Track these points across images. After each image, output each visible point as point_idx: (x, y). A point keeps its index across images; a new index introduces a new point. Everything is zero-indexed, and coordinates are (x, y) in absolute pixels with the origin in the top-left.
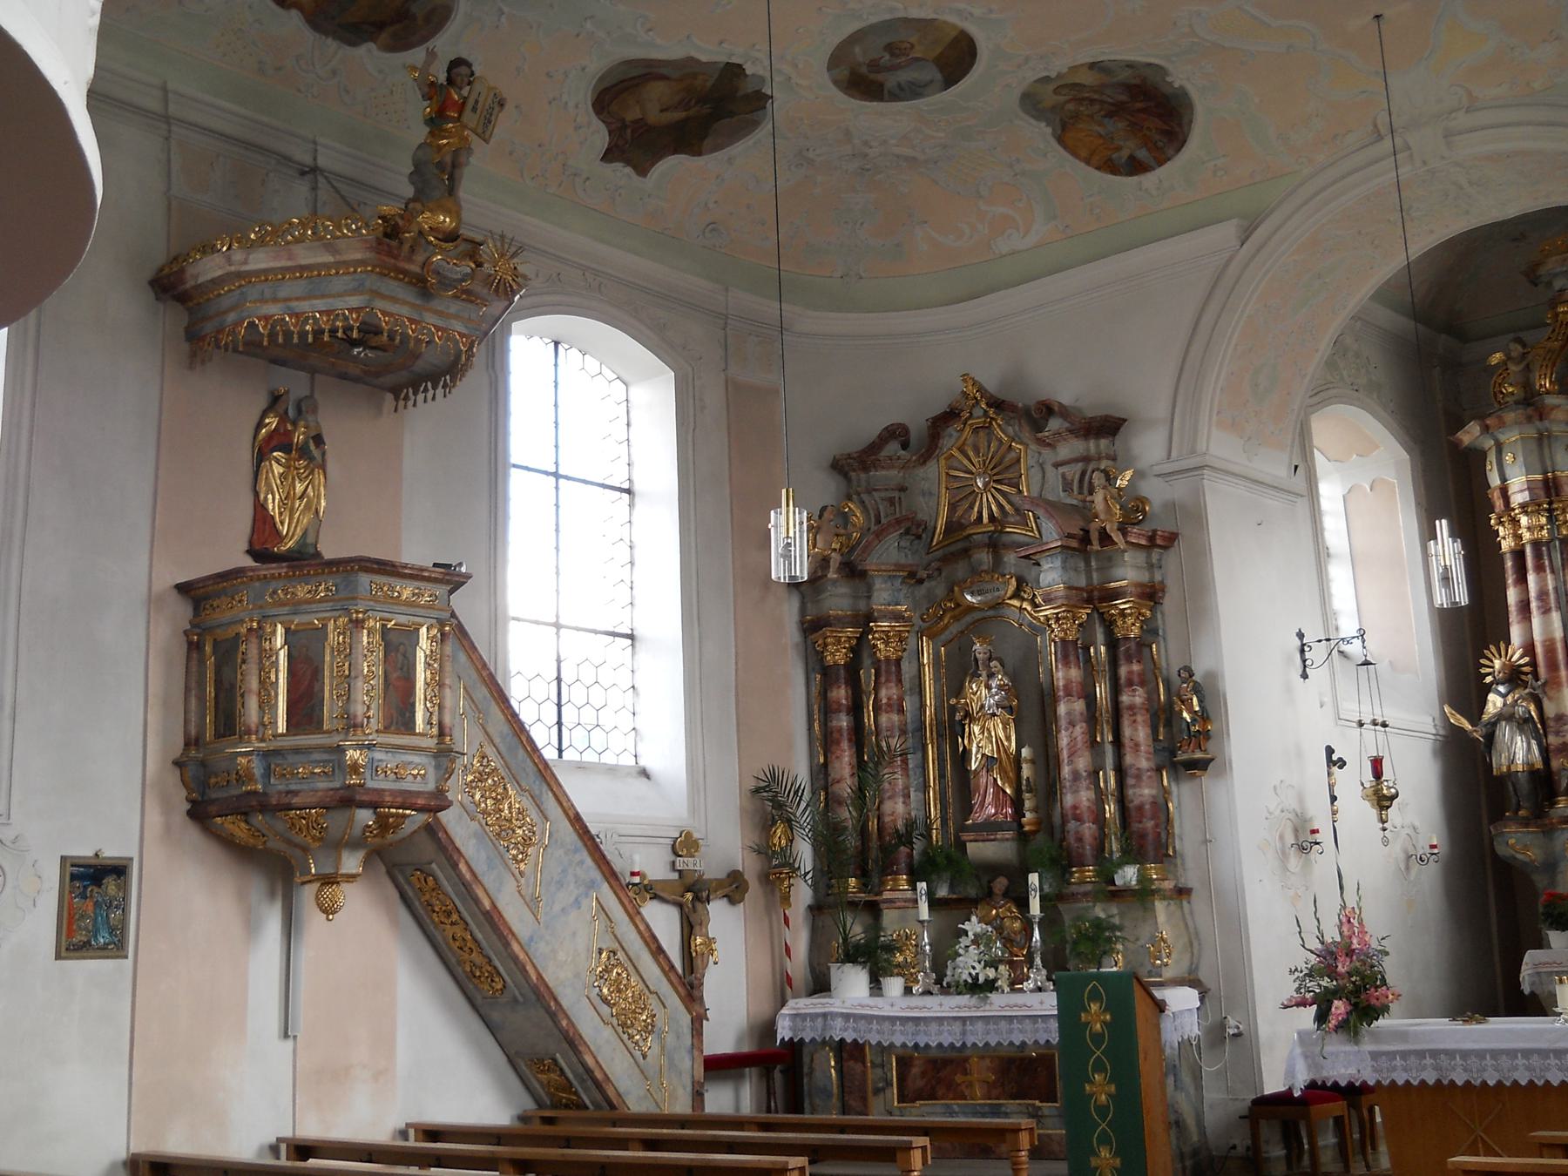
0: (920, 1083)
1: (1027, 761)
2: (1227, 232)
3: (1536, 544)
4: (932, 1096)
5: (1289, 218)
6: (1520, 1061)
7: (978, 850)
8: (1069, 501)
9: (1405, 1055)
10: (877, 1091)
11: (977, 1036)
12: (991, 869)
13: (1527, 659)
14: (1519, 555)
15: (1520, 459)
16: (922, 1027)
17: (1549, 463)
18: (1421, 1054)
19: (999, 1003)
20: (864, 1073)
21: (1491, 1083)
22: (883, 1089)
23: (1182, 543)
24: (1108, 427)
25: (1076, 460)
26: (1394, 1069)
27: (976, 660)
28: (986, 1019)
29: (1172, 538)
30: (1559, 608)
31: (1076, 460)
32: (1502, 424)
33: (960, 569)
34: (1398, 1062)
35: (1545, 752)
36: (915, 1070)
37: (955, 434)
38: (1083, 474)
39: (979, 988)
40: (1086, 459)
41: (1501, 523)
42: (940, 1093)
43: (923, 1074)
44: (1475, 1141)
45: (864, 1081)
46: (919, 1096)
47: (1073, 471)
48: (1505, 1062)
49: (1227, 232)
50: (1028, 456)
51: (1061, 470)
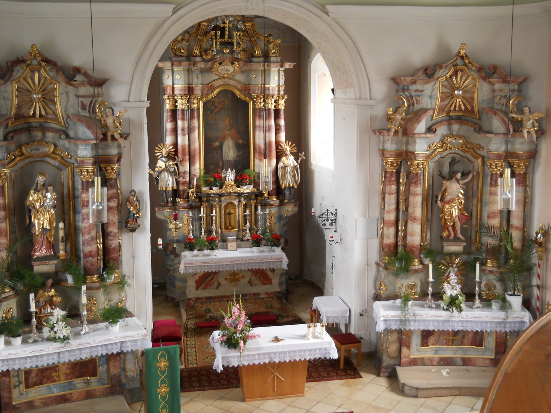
0: (35, 380)
1: (61, 229)
2: (171, 8)
3: (183, 110)
4: (41, 383)
5: (194, 9)
6: (298, 353)
7: (38, 268)
8: (84, 114)
9: (259, 355)
10: (15, 387)
11: (66, 358)
12: (46, 276)
13: (174, 150)
14: (174, 112)
15: (182, 78)
16: (40, 358)
17: (191, 81)
18: (264, 354)
19: (74, 344)
20: (10, 381)
21: (287, 361)
22: (18, 385)
23: (131, 137)
24: (100, 83)
25: (89, 96)
26: (255, 359)
27: (37, 183)
28: (69, 351)
29: (128, 135)
30: (475, 282)
31: (89, 96)
32: (180, 64)
33: (24, 138)
34: (257, 357)
35: (178, 183)
36: (33, 375)
37: (21, 71)
38: (91, 102)
39: (65, 339)
40: (93, 96)
41: (168, 98)
42: (44, 382)
43: (37, 376)
44: (274, 377)
45: (10, 384)
46: (35, 384)
47: (87, 101)
48: (293, 354)
49: (171, 8)
50: (60, 89)
51: (80, 99)
